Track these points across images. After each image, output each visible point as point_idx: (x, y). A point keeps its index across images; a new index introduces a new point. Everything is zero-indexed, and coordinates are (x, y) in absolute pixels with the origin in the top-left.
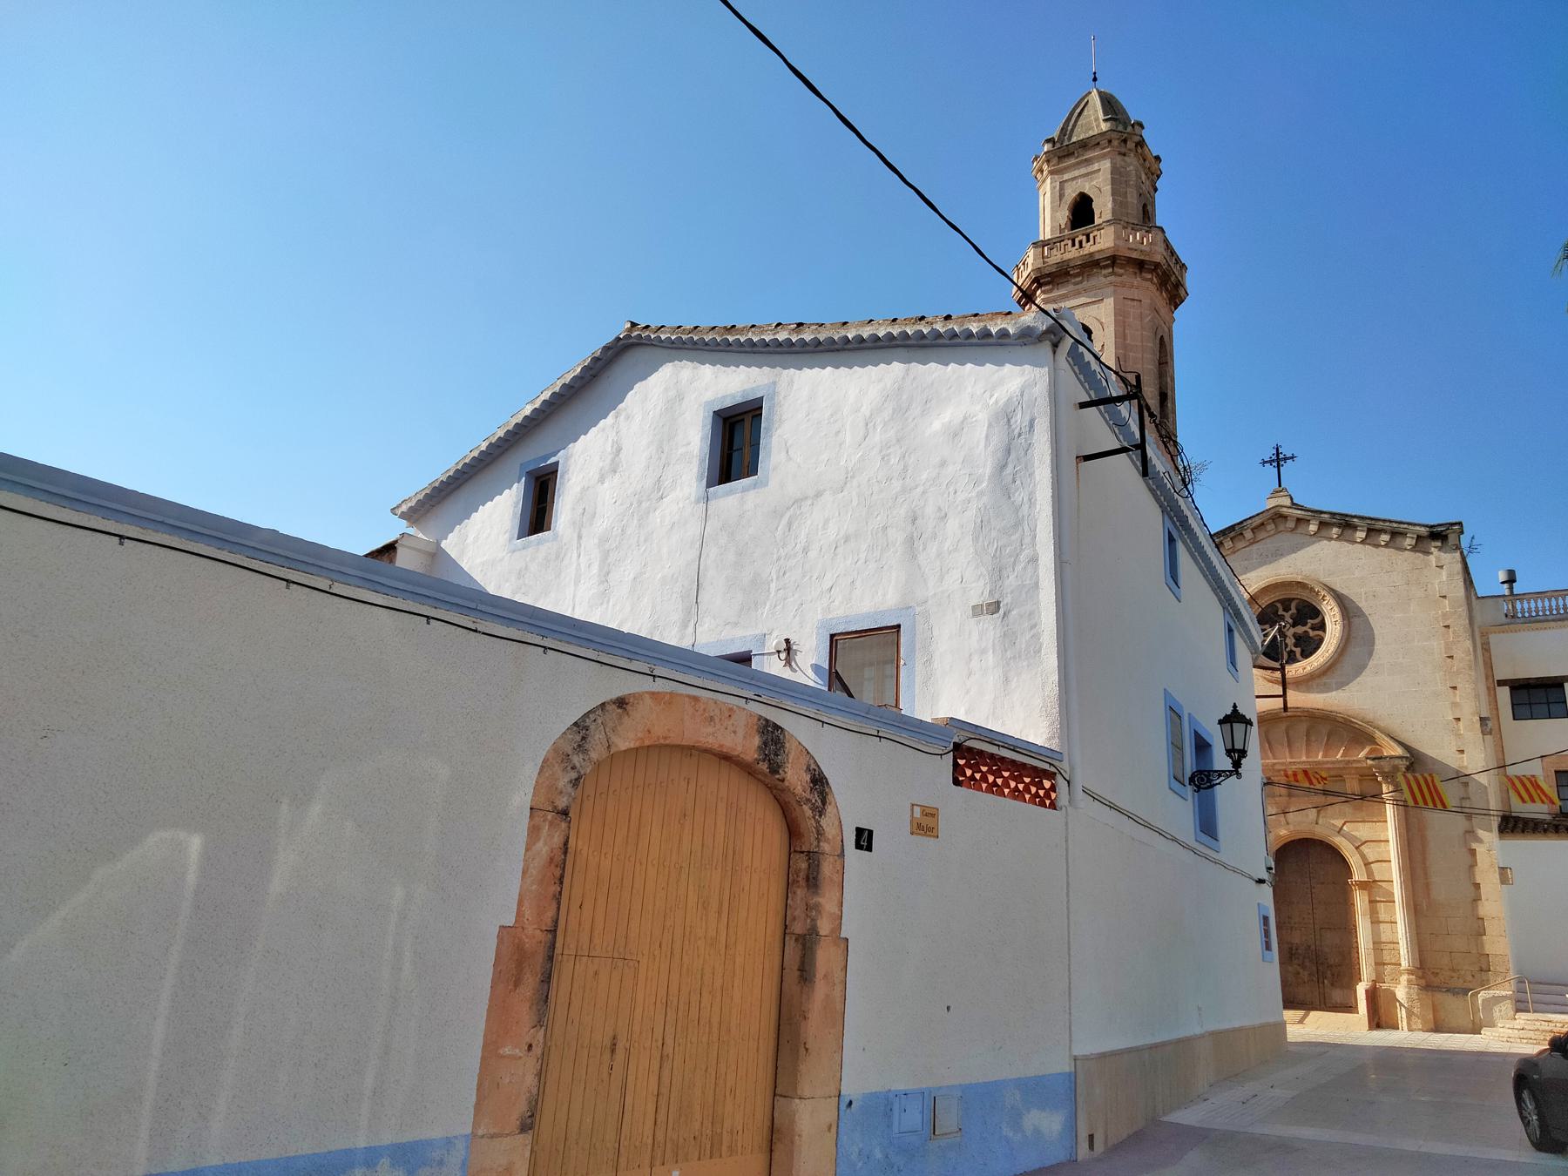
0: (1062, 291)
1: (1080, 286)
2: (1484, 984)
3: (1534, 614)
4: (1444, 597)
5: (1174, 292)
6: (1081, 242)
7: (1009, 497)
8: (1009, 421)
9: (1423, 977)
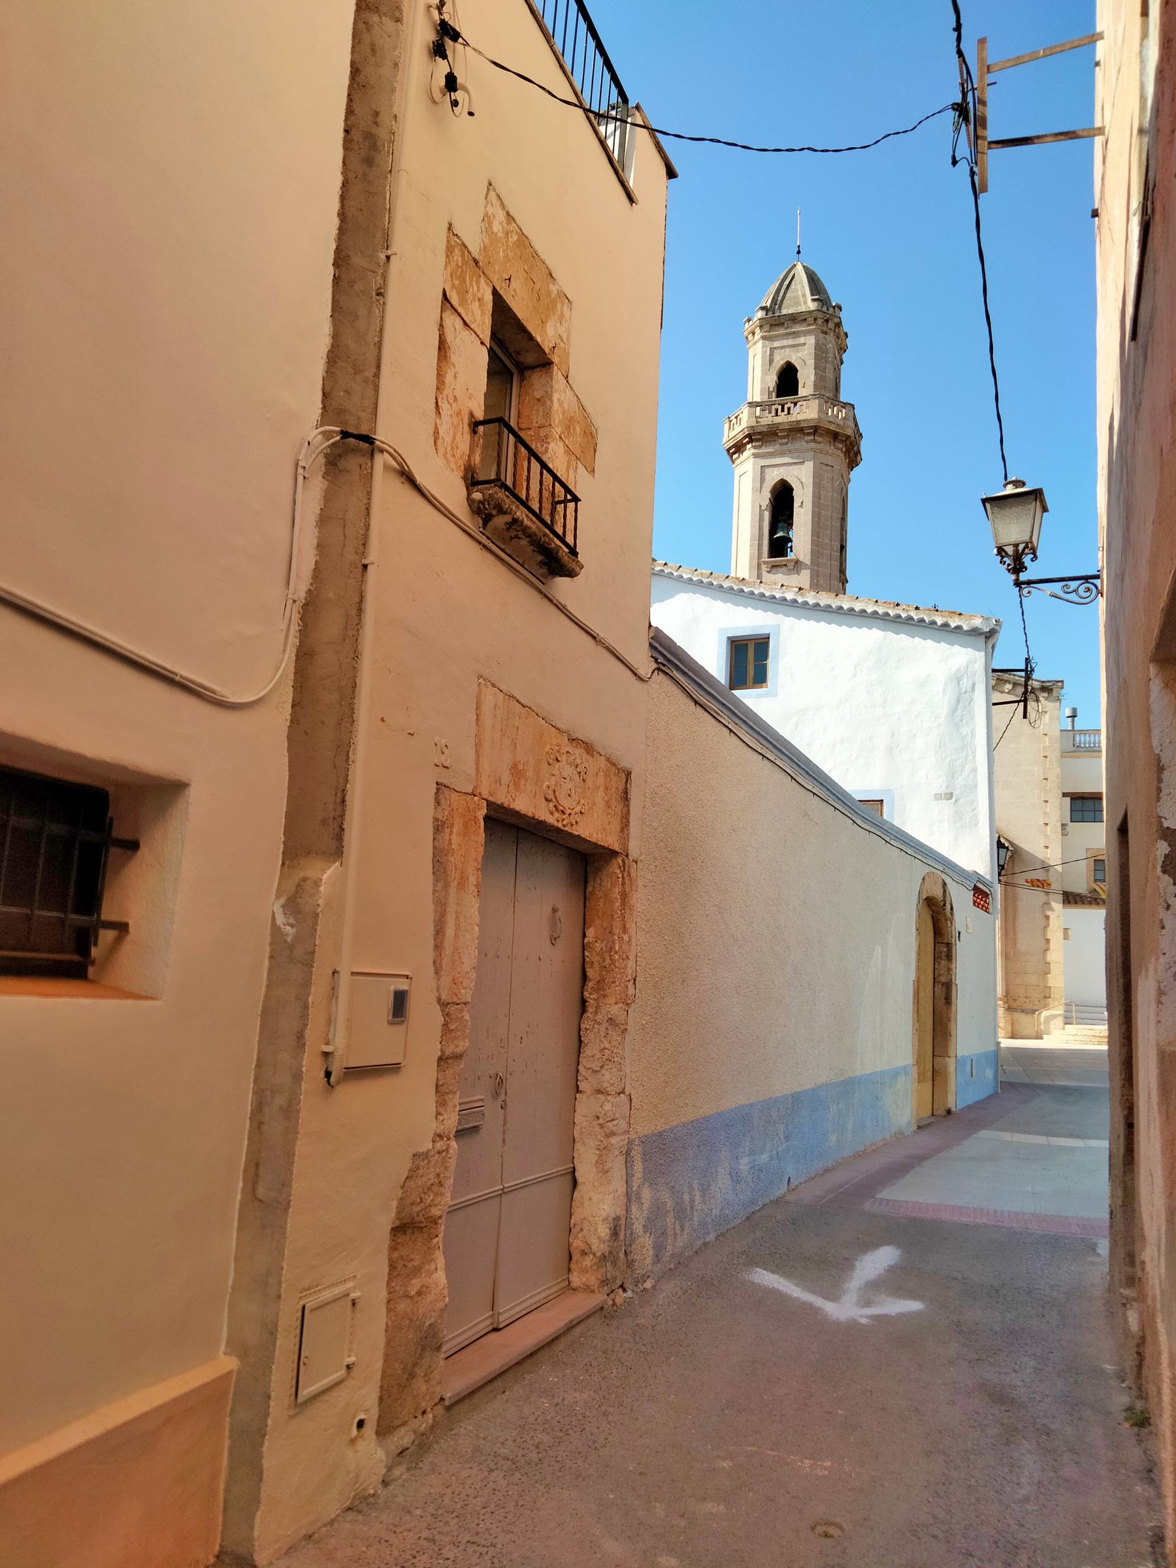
0: (770, 449)
1: (785, 447)
2: (1046, 1007)
3: (1092, 745)
4: (1046, 735)
5: (853, 457)
7: (958, 730)
8: (959, 682)
9: (1006, 1002)
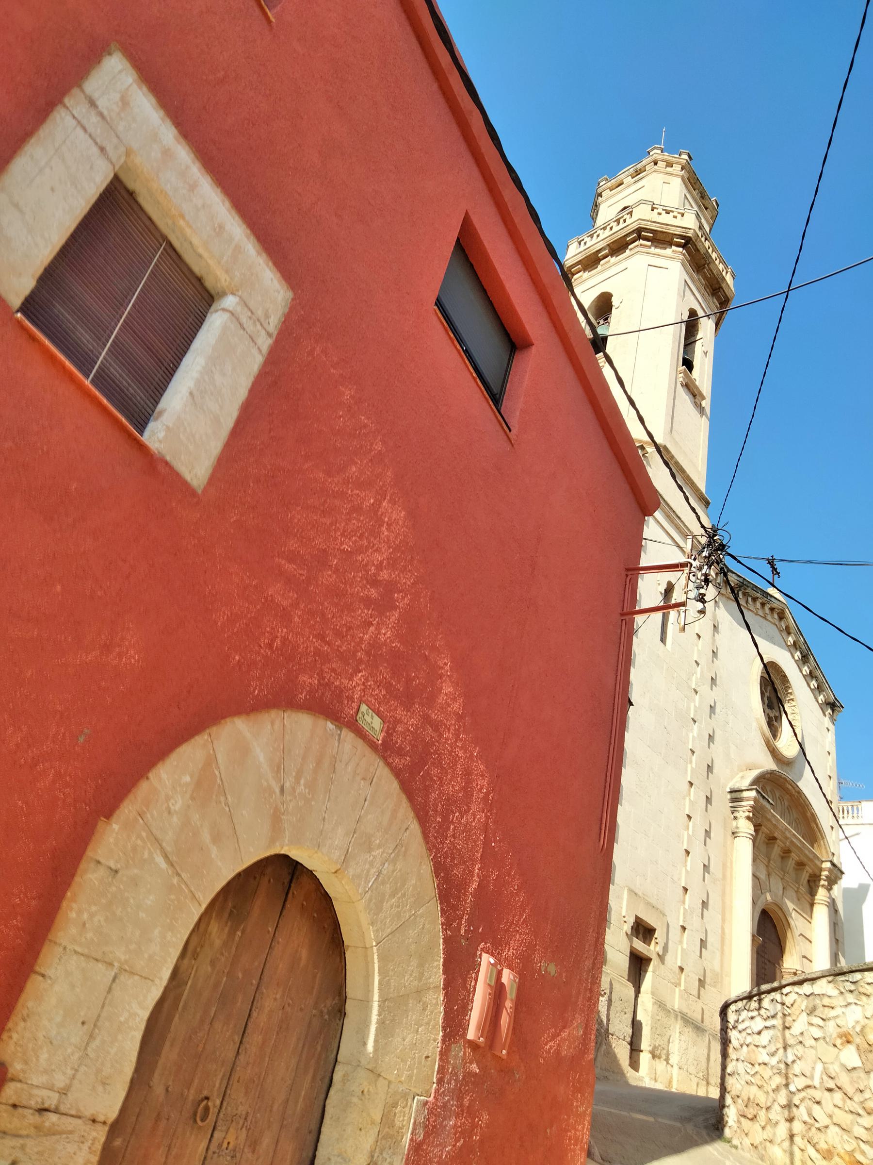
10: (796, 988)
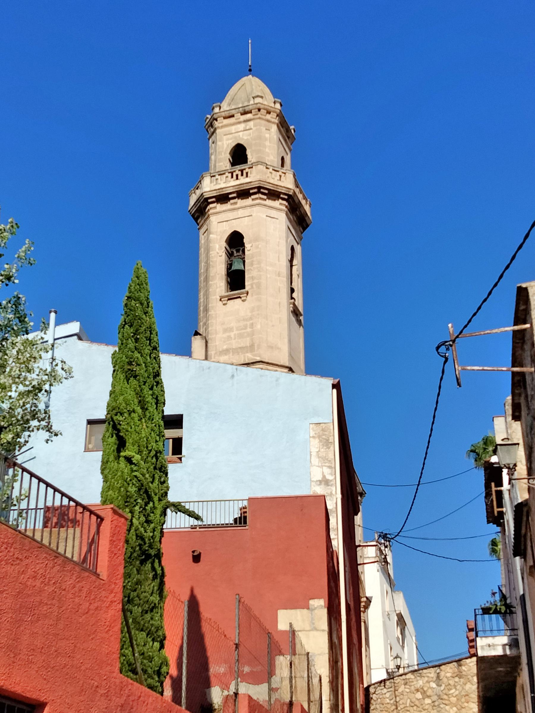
6: (237, 175)
10: (400, 677)
